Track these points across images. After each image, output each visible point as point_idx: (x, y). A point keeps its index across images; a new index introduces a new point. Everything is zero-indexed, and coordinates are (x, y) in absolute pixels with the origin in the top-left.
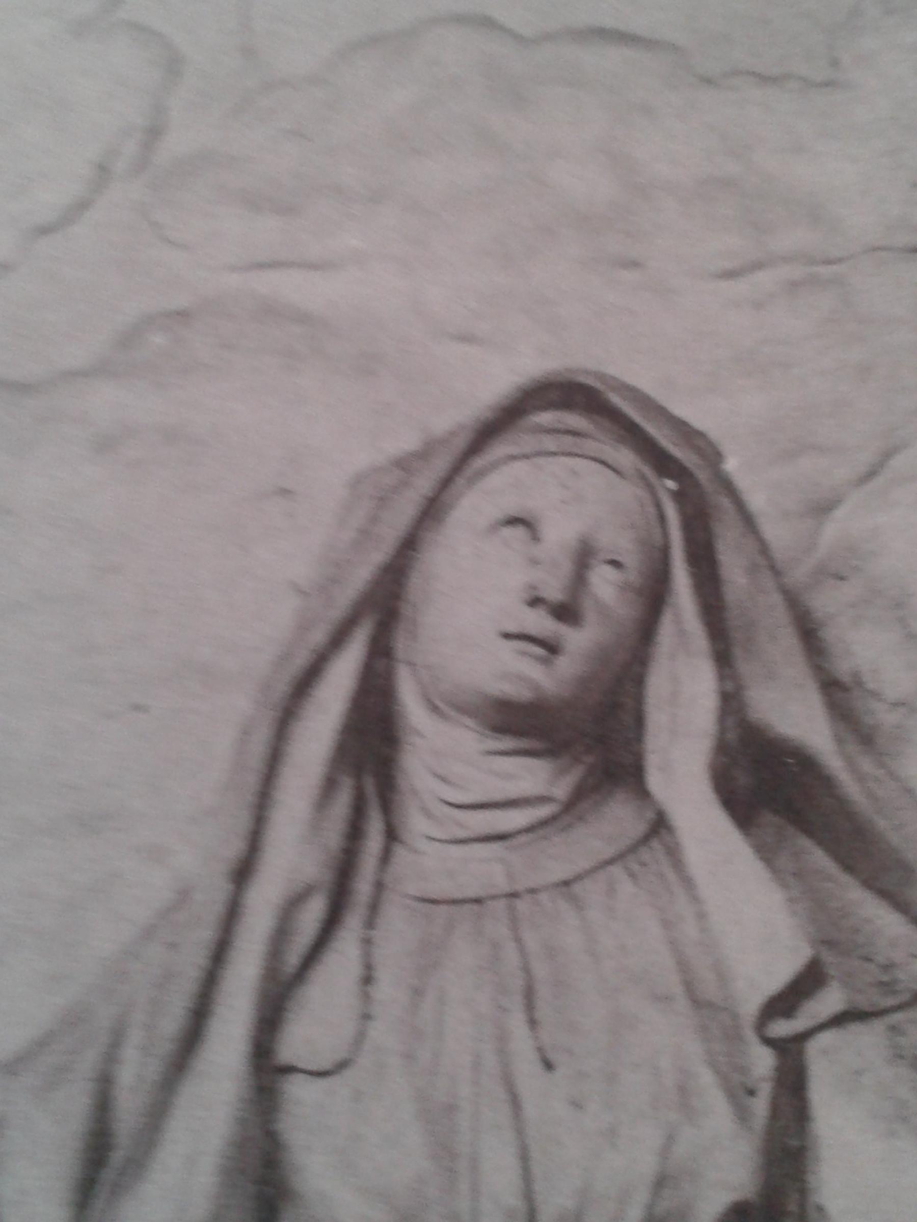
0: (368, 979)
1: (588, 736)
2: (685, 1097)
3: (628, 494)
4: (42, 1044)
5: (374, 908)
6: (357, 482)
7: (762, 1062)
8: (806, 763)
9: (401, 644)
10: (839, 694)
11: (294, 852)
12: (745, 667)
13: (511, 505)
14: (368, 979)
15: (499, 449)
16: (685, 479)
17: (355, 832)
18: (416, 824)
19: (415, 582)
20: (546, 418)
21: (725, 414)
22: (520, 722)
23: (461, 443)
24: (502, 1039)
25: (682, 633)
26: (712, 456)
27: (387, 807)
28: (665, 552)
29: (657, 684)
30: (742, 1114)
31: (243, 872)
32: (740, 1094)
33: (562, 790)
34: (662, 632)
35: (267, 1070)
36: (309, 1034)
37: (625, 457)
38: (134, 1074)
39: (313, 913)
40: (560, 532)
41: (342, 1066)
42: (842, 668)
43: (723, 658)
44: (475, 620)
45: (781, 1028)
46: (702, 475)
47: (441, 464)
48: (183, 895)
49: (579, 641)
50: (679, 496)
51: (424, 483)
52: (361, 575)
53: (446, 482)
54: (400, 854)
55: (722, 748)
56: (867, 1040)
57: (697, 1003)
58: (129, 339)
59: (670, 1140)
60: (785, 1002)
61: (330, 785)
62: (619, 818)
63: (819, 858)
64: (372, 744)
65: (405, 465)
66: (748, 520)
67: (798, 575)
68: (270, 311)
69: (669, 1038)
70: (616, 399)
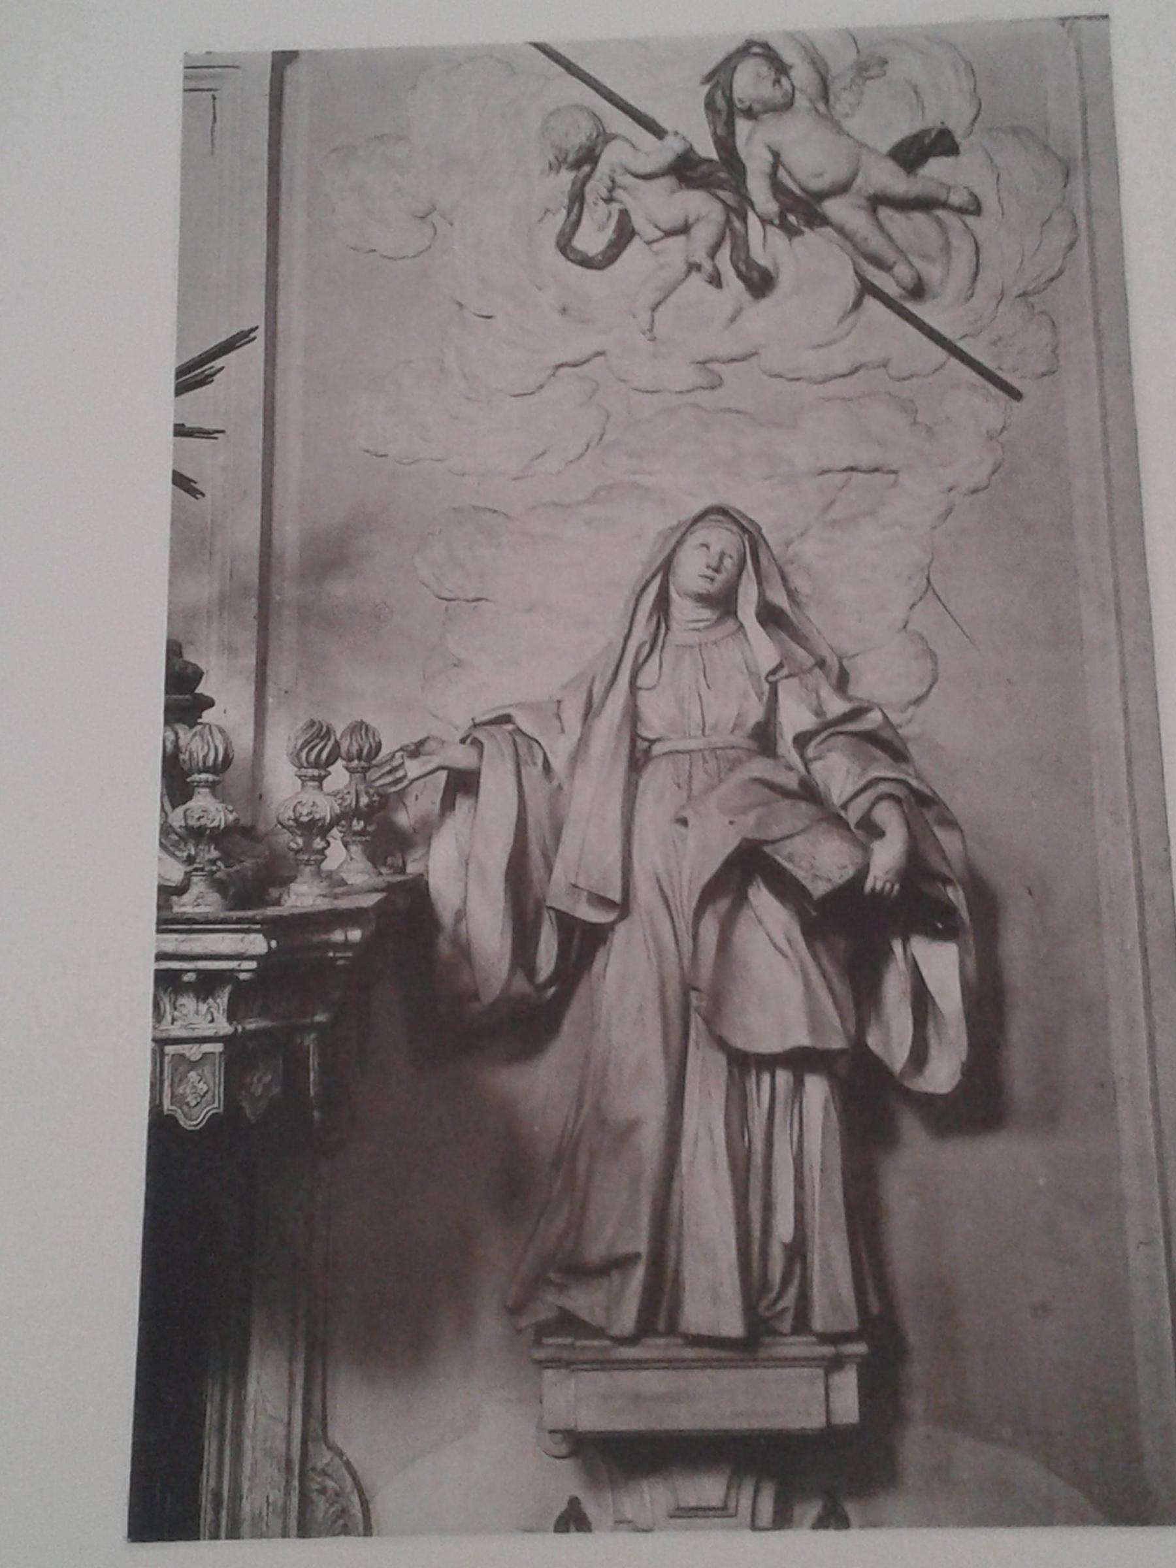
0: (661, 666)
1: (723, 603)
2: (745, 696)
3: (735, 539)
4: (573, 681)
5: (663, 647)
6: (659, 533)
7: (766, 687)
8: (782, 612)
9: (671, 579)
10: (791, 594)
11: (641, 633)
12: (765, 584)
13: (701, 541)
14: (661, 666)
15: (700, 525)
16: (753, 539)
17: (658, 627)
18: (674, 625)
19: (675, 560)
20: (713, 517)
21: (764, 518)
22: (703, 599)
23: (689, 523)
24: (697, 681)
25: (748, 575)
26: (759, 529)
27: (666, 621)
28: (745, 553)
29: (741, 590)
30: (760, 699)
31: (627, 638)
32: (760, 695)
33: (715, 617)
34: (664, 1108)
35: (633, 688)
36: (644, 680)
37: (735, 529)
38: (598, 689)
39: (646, 649)
40: (715, 549)
41: (654, 687)
42: (792, 586)
43: (760, 583)
44: (692, 571)
45: (771, 678)
46: (756, 534)
47: (683, 529)
48: (610, 643)
49: (720, 578)
50: (750, 540)
51: (678, 534)
52: (659, 560)
53: (684, 534)
54: (670, 633)
55: (759, 605)
56: (794, 681)
57: (750, 673)
58: (595, 493)
59: (741, 706)
60: (773, 672)
61: (651, 615)
62: (730, 625)
63: (783, 635)
64: (663, 604)
65: (673, 529)
66: (768, 547)
67: (780, 562)
68: (636, 486)
69: (741, 681)
70: (732, 512)
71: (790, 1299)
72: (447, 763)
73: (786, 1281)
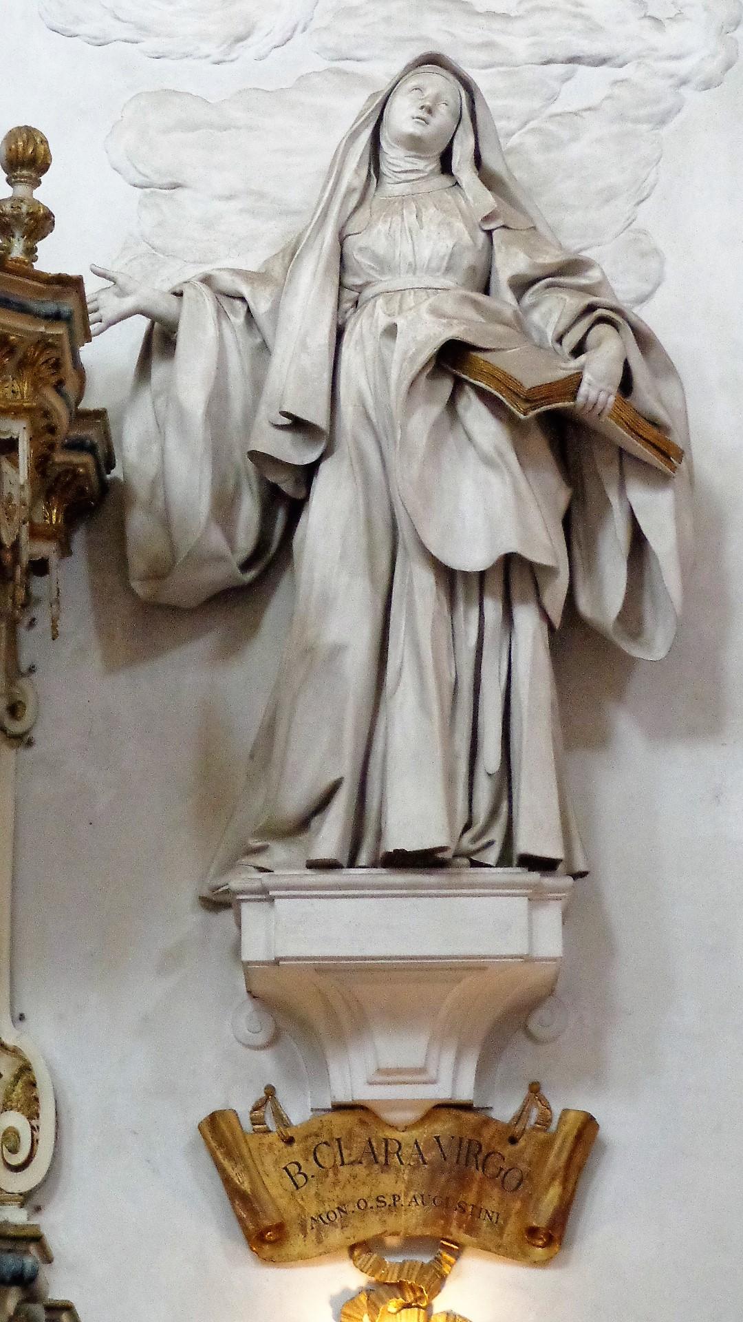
22: (415, 144)
39: (355, 199)
40: (430, 92)
71: (497, 834)
72: (143, 304)
73: (494, 813)
